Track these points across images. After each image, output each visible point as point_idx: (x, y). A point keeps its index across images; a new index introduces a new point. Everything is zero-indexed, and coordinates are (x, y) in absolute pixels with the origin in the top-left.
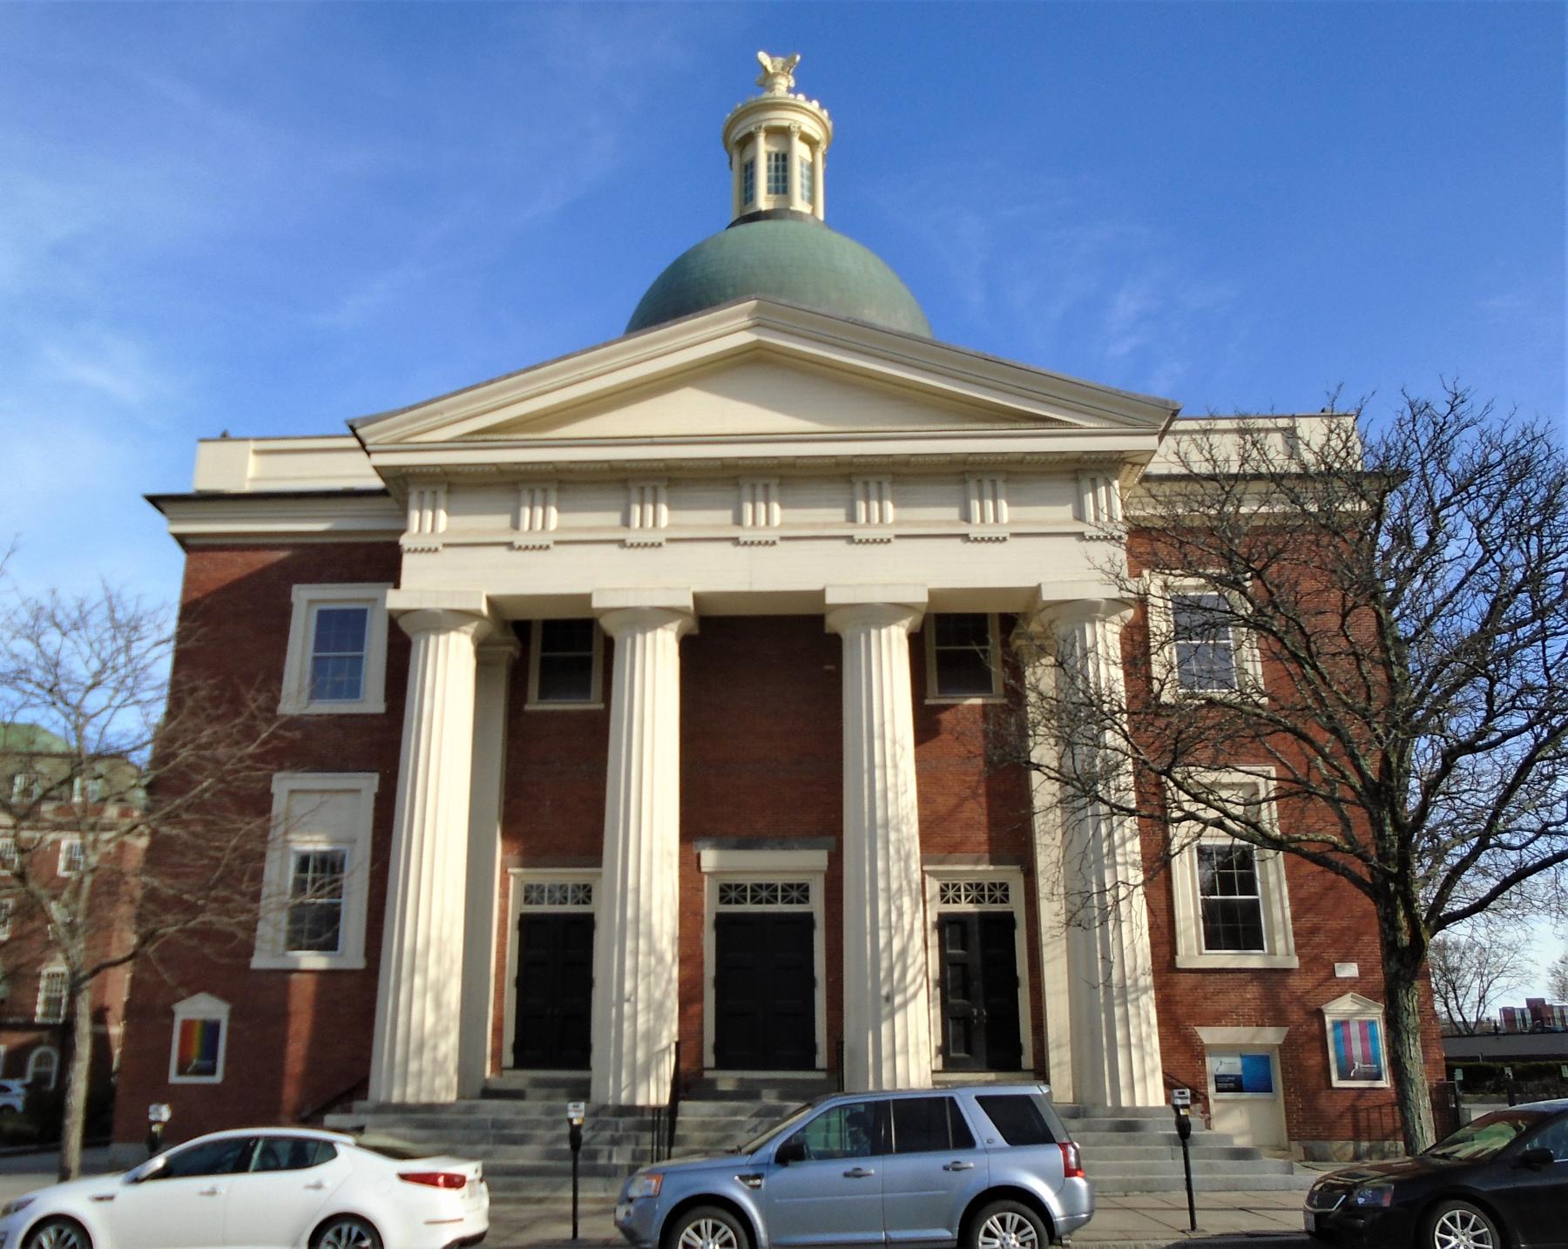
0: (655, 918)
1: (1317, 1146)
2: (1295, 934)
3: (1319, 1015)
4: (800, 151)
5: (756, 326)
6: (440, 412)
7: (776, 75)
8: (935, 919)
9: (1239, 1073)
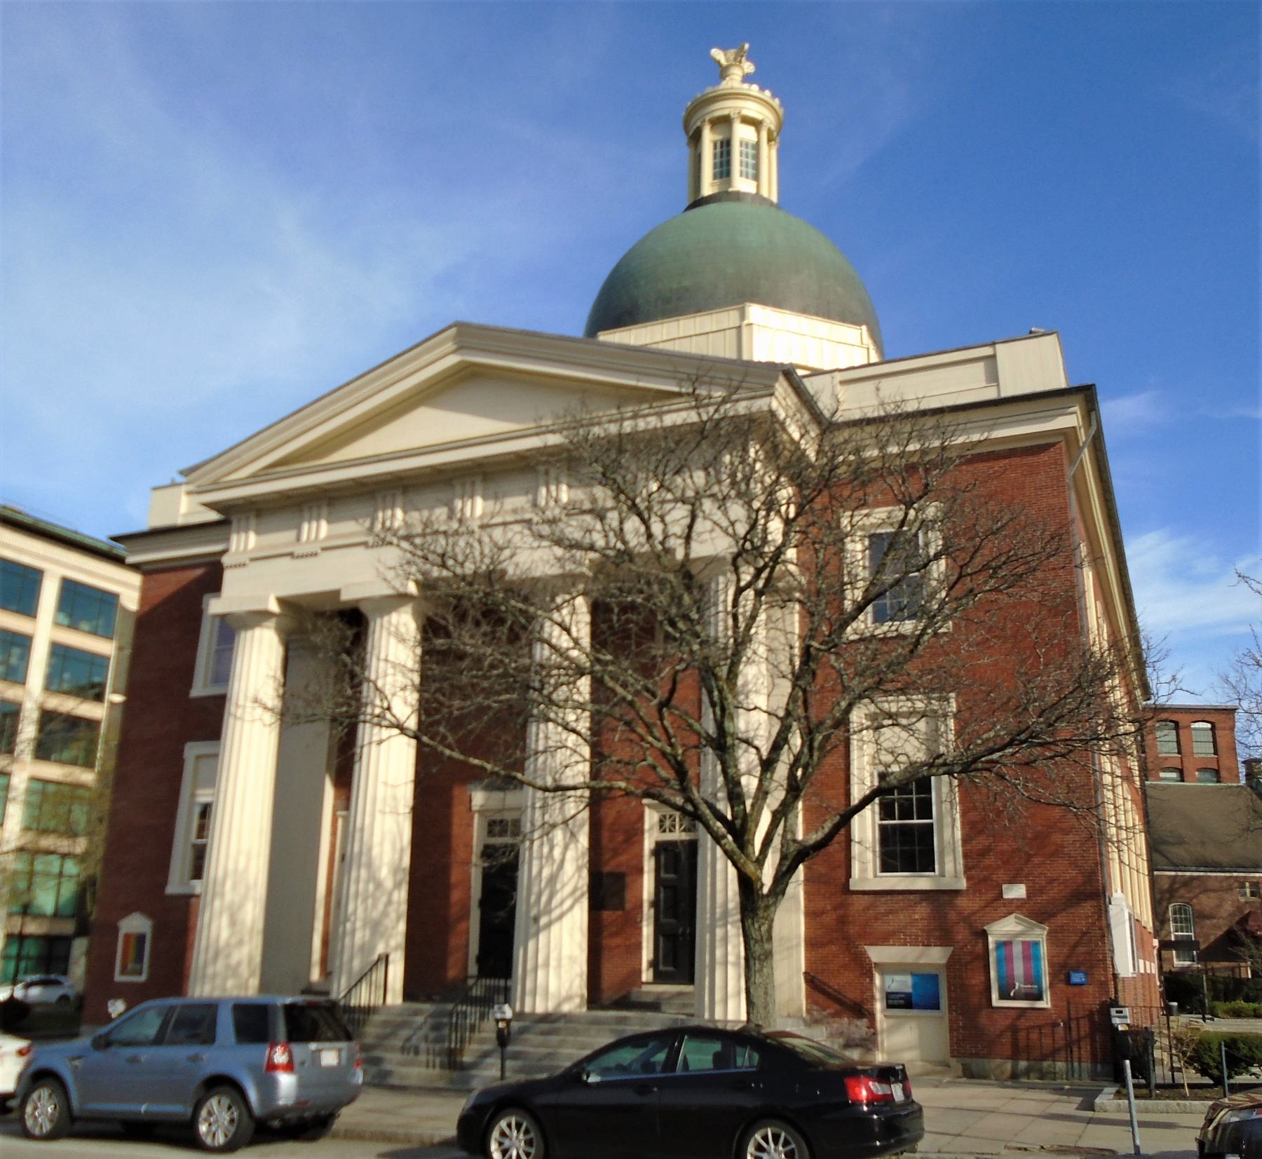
0: (375, 851)
1: (975, 1064)
2: (965, 856)
3: (984, 935)
4: (742, 133)
5: (460, 349)
6: (238, 456)
7: (728, 67)
8: (653, 846)
9: (910, 990)
